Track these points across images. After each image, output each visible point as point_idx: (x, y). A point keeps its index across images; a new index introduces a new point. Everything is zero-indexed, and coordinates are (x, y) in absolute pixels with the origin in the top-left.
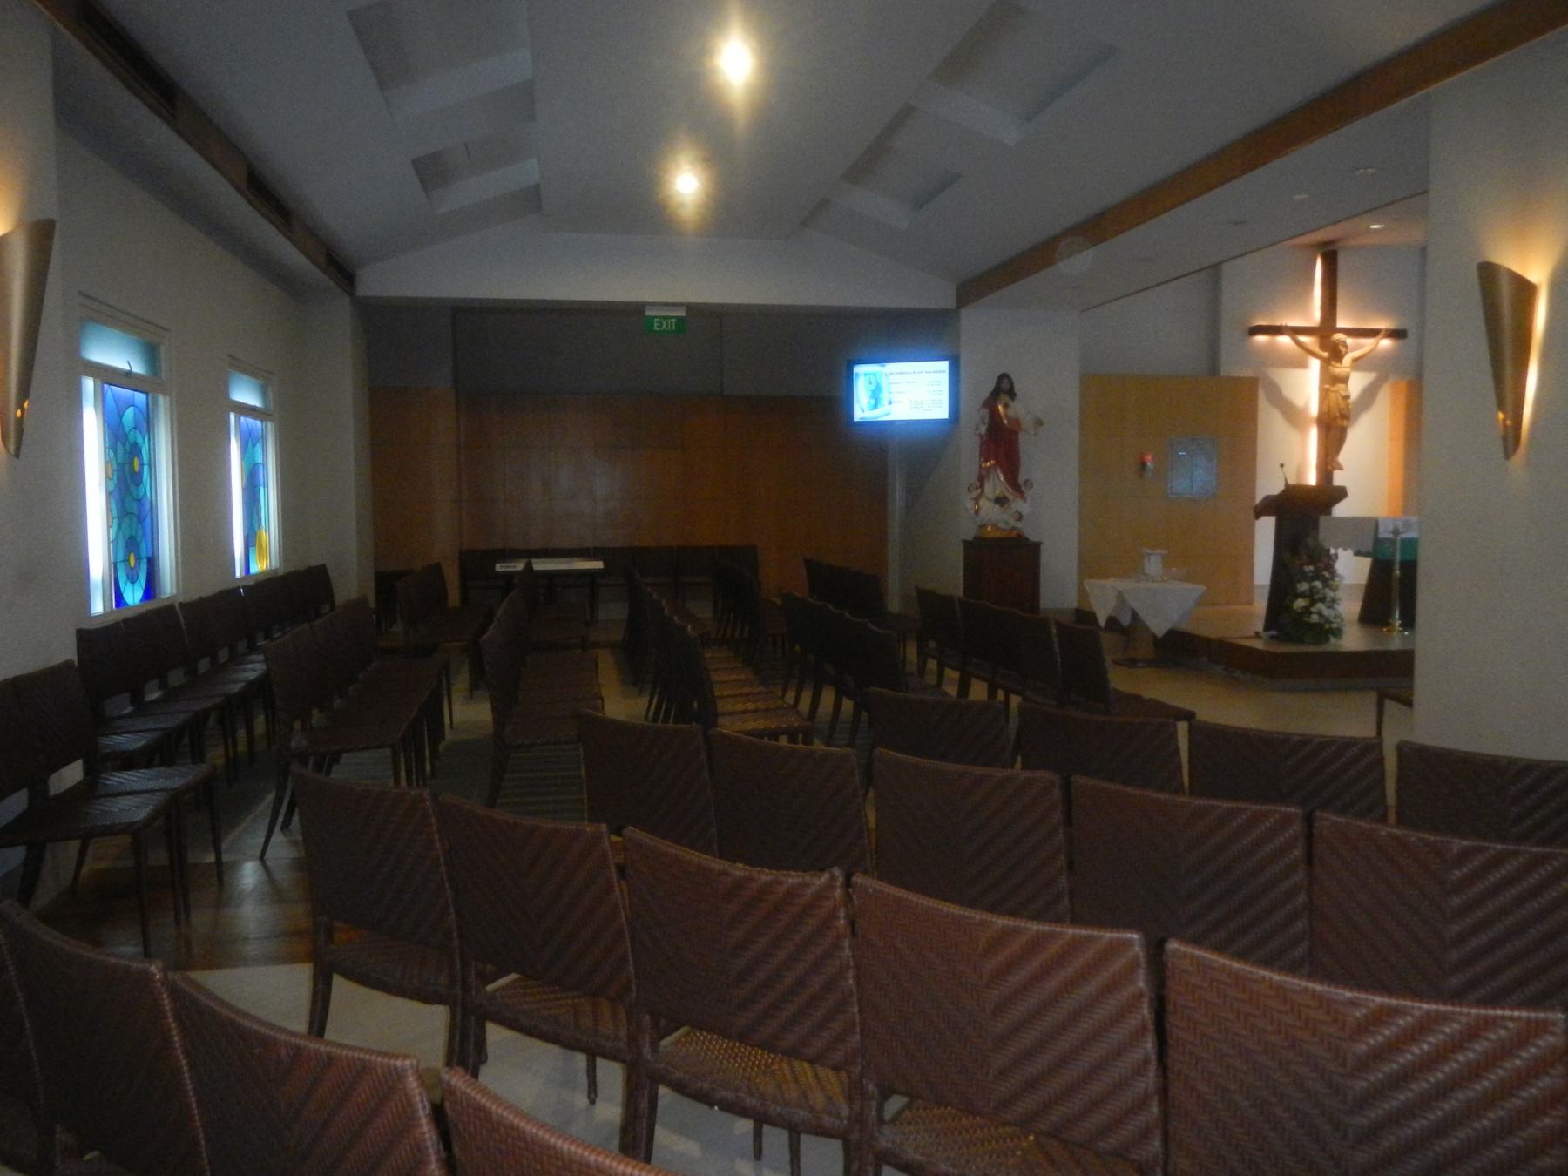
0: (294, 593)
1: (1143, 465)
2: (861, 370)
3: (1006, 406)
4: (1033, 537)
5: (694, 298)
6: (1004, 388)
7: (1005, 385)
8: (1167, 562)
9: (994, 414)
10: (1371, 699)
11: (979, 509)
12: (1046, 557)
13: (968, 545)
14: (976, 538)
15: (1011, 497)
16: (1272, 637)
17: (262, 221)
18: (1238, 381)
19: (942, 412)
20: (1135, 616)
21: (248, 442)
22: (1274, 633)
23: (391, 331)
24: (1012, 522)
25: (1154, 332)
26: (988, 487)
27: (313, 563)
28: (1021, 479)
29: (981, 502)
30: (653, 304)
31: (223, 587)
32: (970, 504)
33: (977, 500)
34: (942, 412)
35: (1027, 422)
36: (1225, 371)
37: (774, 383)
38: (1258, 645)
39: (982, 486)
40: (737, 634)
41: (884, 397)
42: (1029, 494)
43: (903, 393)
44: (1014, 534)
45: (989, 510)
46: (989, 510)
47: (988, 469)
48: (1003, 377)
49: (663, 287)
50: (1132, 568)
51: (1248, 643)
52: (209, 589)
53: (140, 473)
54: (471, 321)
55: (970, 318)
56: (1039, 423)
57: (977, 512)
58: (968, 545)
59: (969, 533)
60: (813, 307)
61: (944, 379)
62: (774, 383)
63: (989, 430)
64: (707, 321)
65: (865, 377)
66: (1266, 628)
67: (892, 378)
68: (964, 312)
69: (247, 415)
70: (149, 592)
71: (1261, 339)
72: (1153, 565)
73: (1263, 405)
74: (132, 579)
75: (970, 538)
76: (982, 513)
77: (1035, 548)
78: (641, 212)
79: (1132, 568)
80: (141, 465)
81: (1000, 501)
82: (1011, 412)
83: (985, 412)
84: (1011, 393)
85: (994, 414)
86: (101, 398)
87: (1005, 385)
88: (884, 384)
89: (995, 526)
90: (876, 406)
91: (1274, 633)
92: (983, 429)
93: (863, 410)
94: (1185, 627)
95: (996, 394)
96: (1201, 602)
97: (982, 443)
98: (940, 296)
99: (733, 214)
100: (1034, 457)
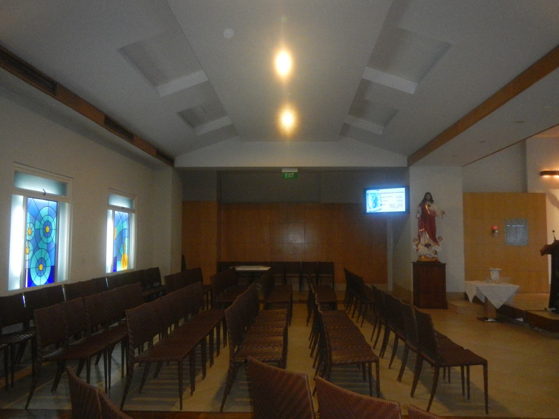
0: (142, 280)
1: (493, 231)
2: (369, 192)
3: (429, 206)
4: (442, 261)
5: (300, 165)
6: (428, 198)
7: (428, 197)
8: (501, 273)
9: (424, 210)
10: (252, 411)
11: (419, 249)
12: (449, 270)
13: (415, 264)
14: (418, 261)
15: (432, 244)
16: (553, 311)
17: (120, 139)
18: (535, 195)
19: (403, 209)
20: (486, 298)
21: (117, 222)
22: (554, 309)
23: (190, 179)
24: (433, 255)
25: (496, 174)
26: (422, 240)
27: (154, 267)
28: (437, 236)
29: (419, 246)
30: (284, 168)
31: (96, 276)
32: (414, 247)
33: (417, 245)
34: (403, 209)
35: (438, 212)
36: (530, 190)
37: (331, 197)
38: (546, 315)
39: (419, 240)
40: (206, 309)
41: (379, 203)
42: (441, 243)
43: (387, 201)
44: (433, 260)
45: (423, 250)
46: (423, 250)
47: (422, 232)
48: (428, 194)
49: (288, 161)
50: (486, 277)
51: (539, 314)
52: (87, 276)
53: (50, 233)
54: (224, 176)
55: (414, 171)
56: (443, 213)
57: (417, 250)
58: (415, 264)
59: (415, 259)
60: (334, 168)
61: (403, 195)
62: (331, 197)
63: (422, 216)
64: (302, 171)
65: (371, 195)
66: (550, 307)
67: (382, 195)
68: (410, 167)
69: (118, 211)
70: (51, 279)
71: (546, 177)
72: (495, 275)
73: (549, 206)
74: (40, 273)
75: (415, 261)
76: (419, 251)
77: (444, 266)
78: (267, 130)
79: (486, 277)
80: (51, 230)
81: (427, 246)
82: (431, 208)
83: (420, 208)
84: (432, 201)
85: (424, 210)
86: (26, 205)
87: (428, 197)
88: (379, 197)
89: (425, 256)
90: (375, 207)
91: (554, 309)
92: (419, 216)
93: (370, 208)
94: (512, 304)
95: (425, 200)
96: (518, 292)
97: (419, 221)
98: (399, 161)
99: (309, 131)
100: (442, 228)
